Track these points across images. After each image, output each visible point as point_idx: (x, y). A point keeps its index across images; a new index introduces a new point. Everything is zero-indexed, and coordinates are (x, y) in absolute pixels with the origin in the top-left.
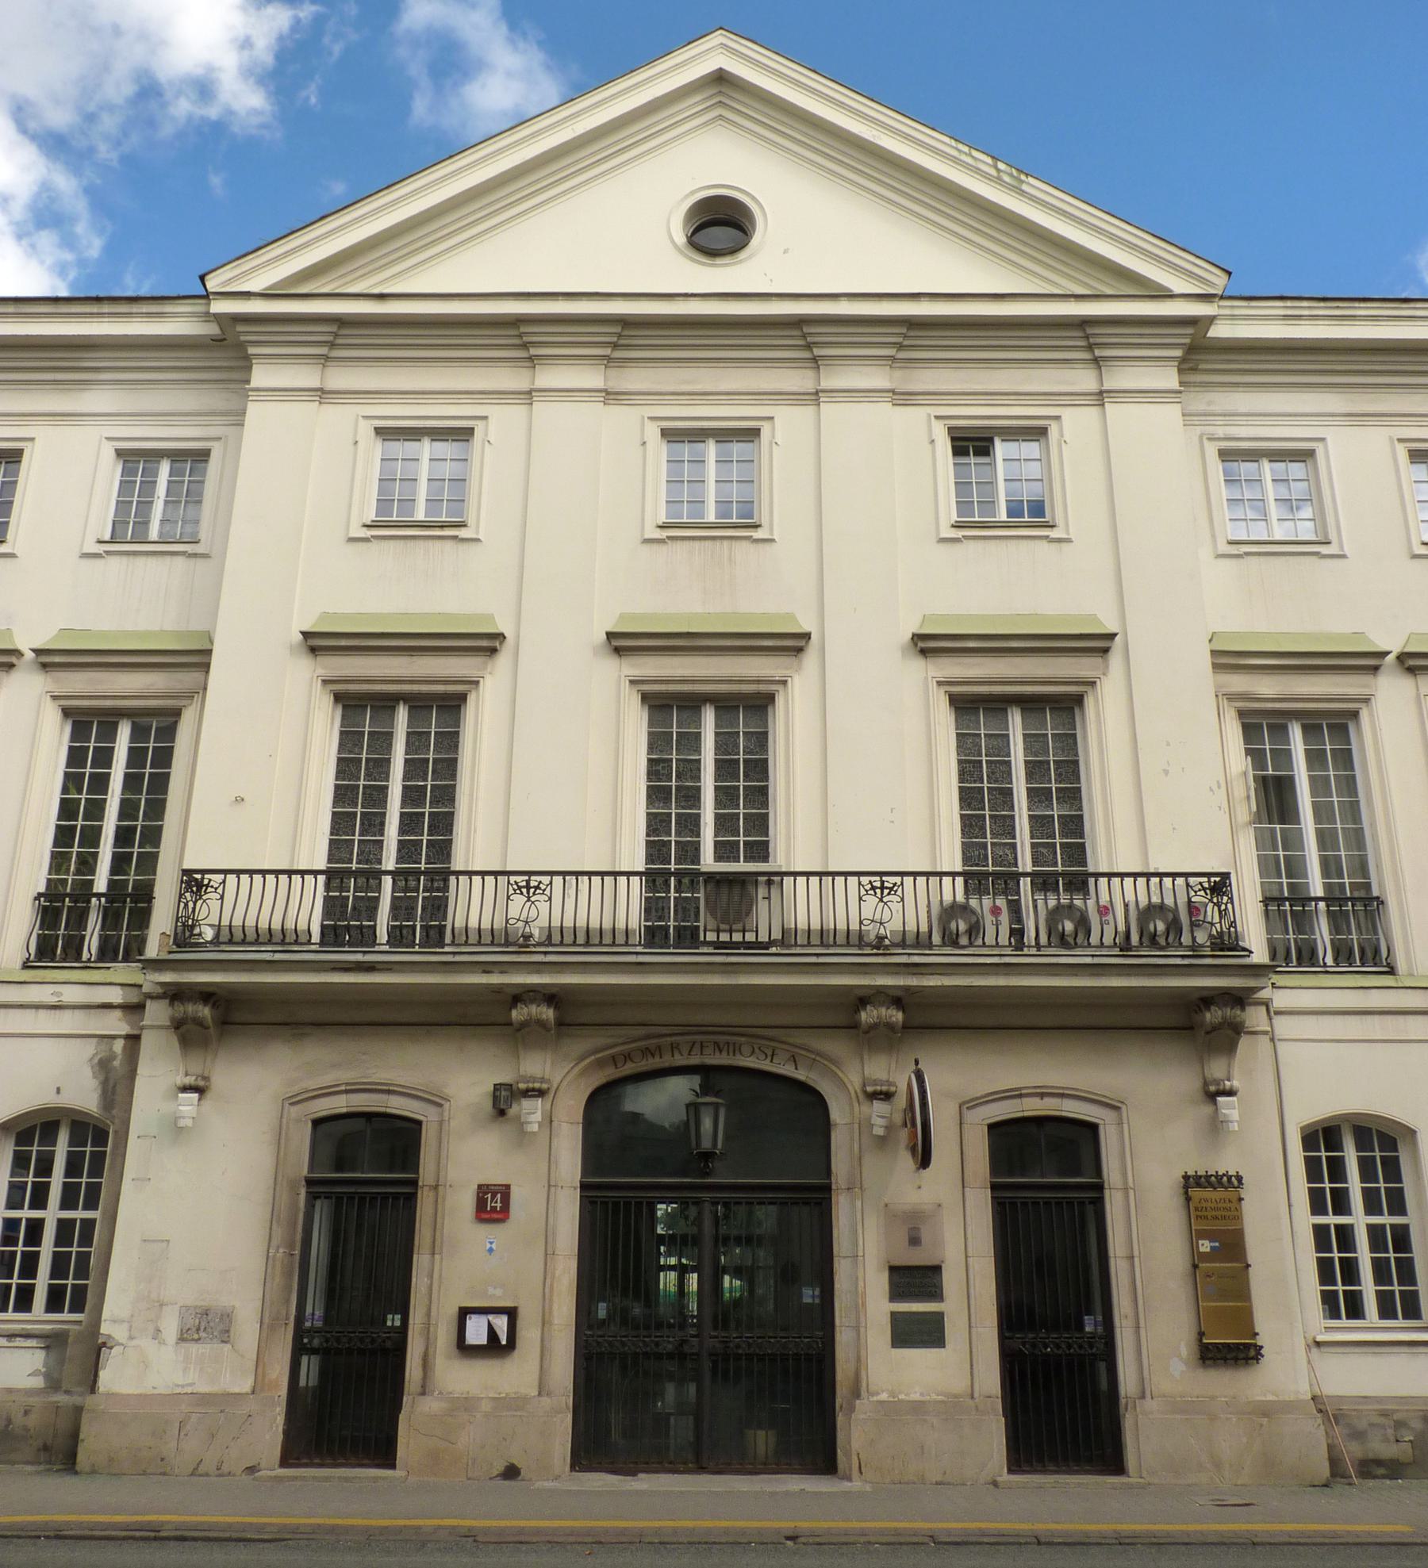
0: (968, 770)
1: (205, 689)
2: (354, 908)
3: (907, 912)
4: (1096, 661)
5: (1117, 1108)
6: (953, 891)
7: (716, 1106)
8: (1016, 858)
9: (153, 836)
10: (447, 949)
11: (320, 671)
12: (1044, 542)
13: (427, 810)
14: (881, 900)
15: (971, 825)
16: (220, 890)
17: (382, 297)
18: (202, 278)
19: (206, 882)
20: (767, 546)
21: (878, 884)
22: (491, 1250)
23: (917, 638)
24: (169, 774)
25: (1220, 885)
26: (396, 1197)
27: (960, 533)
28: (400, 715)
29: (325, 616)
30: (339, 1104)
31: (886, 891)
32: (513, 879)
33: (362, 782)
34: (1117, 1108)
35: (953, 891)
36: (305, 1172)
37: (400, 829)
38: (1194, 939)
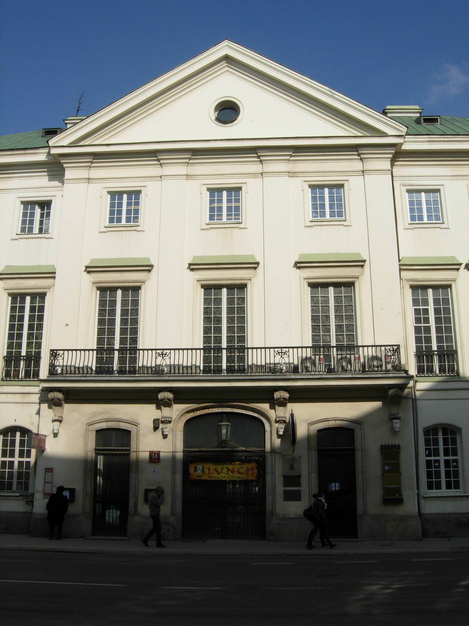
0: (314, 309)
1: (54, 285)
2: (106, 361)
3: (294, 358)
4: (359, 269)
5: (360, 424)
6: (308, 353)
7: (227, 425)
8: (330, 340)
9: (39, 337)
10: (137, 375)
11: (92, 280)
12: (342, 226)
13: (129, 327)
14: (281, 357)
15: (315, 329)
16: (62, 356)
17: (108, 145)
18: (47, 142)
19: (58, 354)
20: (245, 229)
21: (280, 351)
22: (154, 472)
23: (296, 263)
24: (43, 315)
25: (396, 349)
26: (124, 455)
27: (312, 224)
28: (119, 300)
29: (93, 260)
30: (104, 425)
31: (283, 354)
32: (158, 351)
33: (107, 318)
34: (360, 424)
35: (308, 353)
36: (94, 447)
37: (120, 333)
38: (386, 368)
